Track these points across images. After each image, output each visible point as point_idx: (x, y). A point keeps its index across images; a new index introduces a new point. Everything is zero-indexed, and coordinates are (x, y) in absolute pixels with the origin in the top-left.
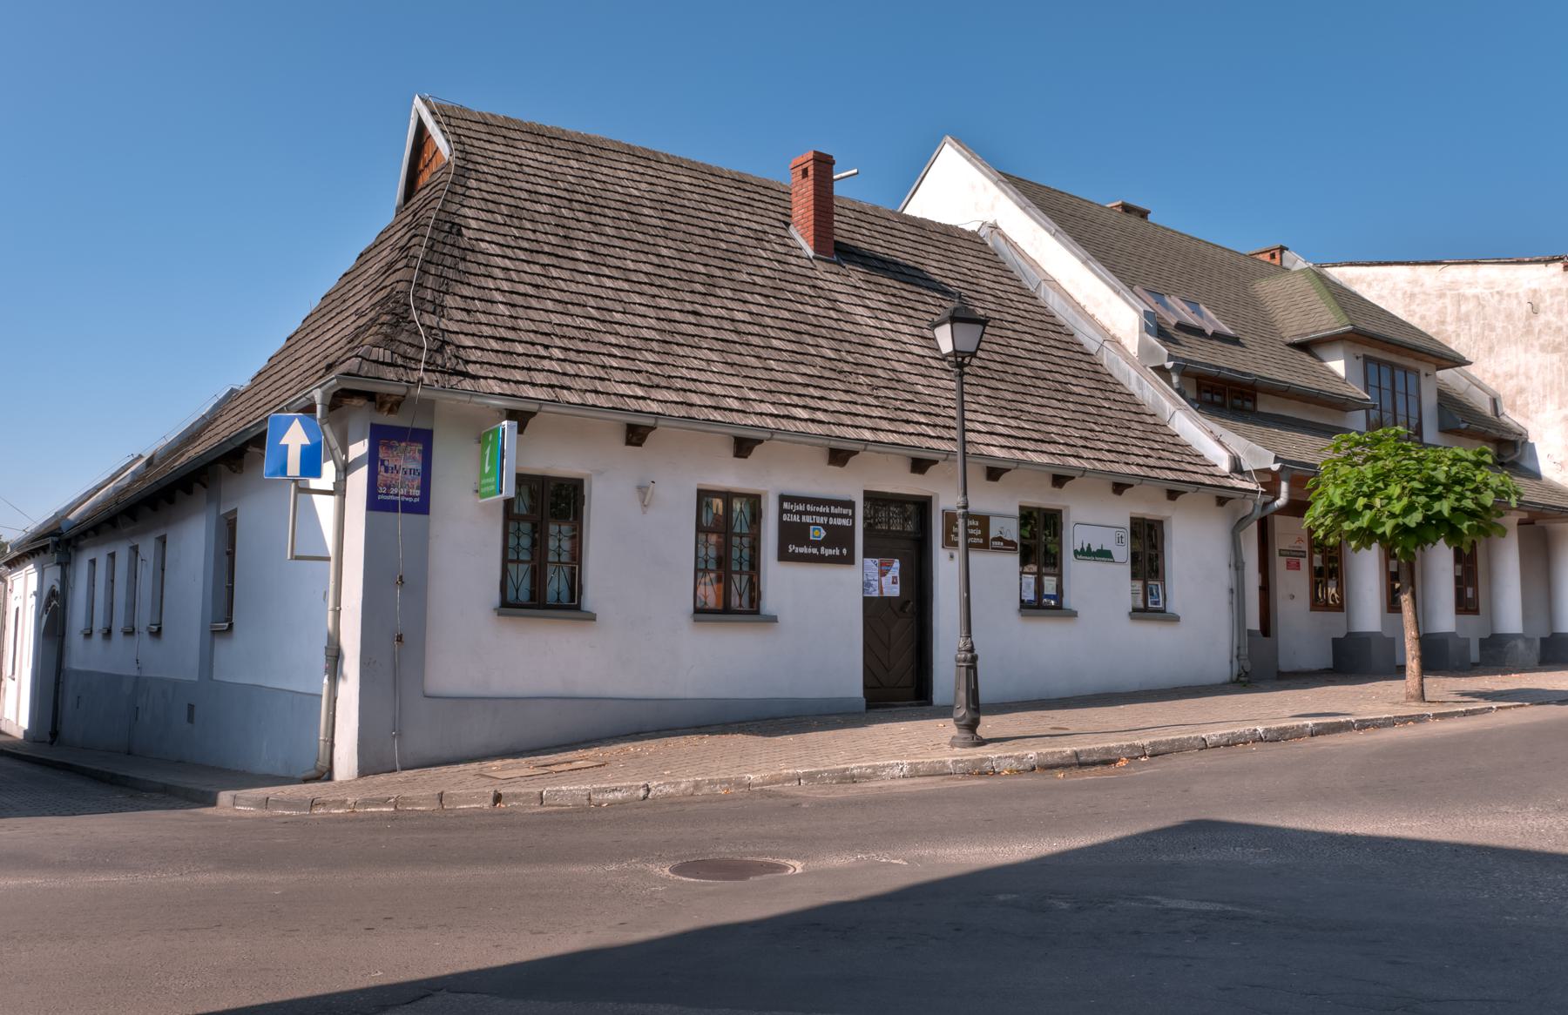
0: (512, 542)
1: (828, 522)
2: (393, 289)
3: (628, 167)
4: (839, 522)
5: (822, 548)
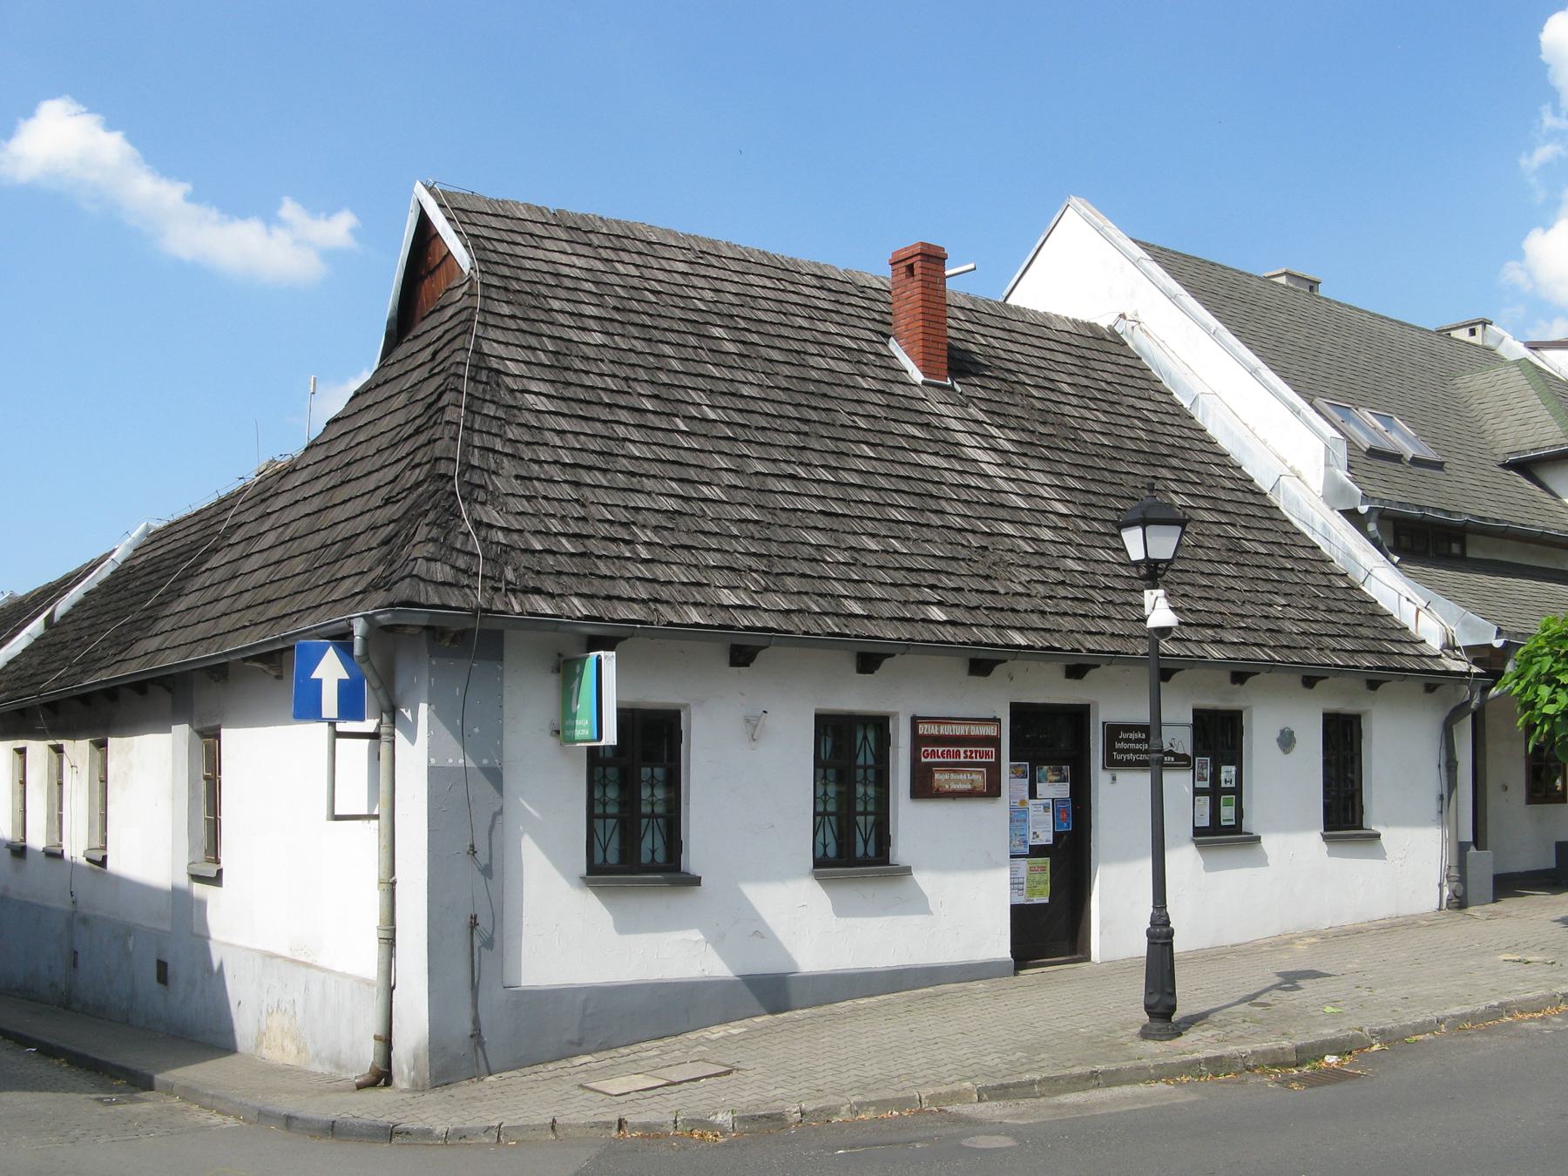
0: (598, 795)
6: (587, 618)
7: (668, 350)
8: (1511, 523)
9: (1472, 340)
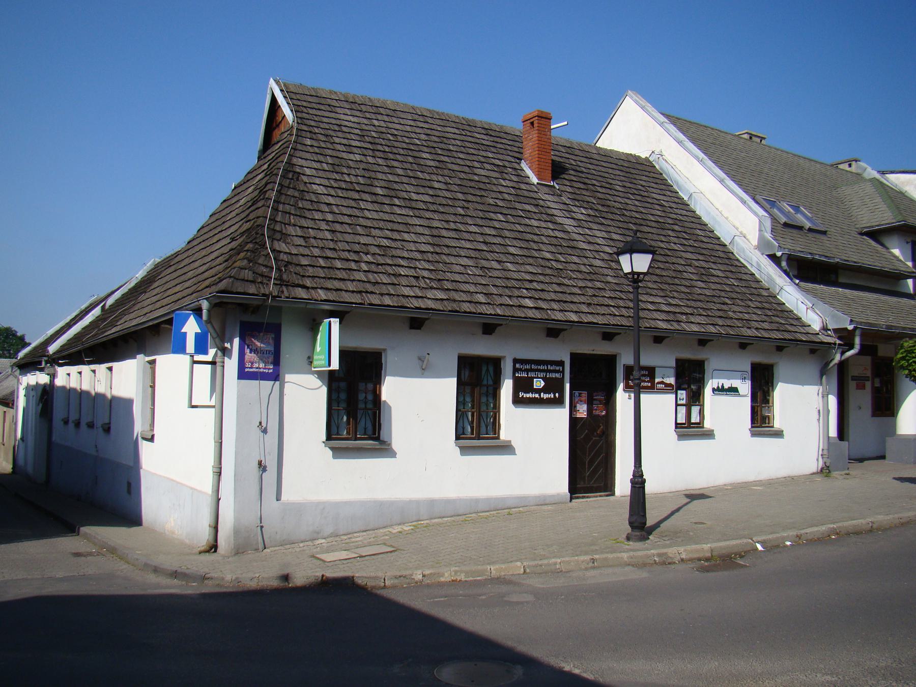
1: (546, 375)
2: (254, 223)
3: (412, 123)
4: (554, 375)
5: (542, 394)
6: (325, 301)
7: (395, 164)
8: (863, 264)
9: (848, 169)
